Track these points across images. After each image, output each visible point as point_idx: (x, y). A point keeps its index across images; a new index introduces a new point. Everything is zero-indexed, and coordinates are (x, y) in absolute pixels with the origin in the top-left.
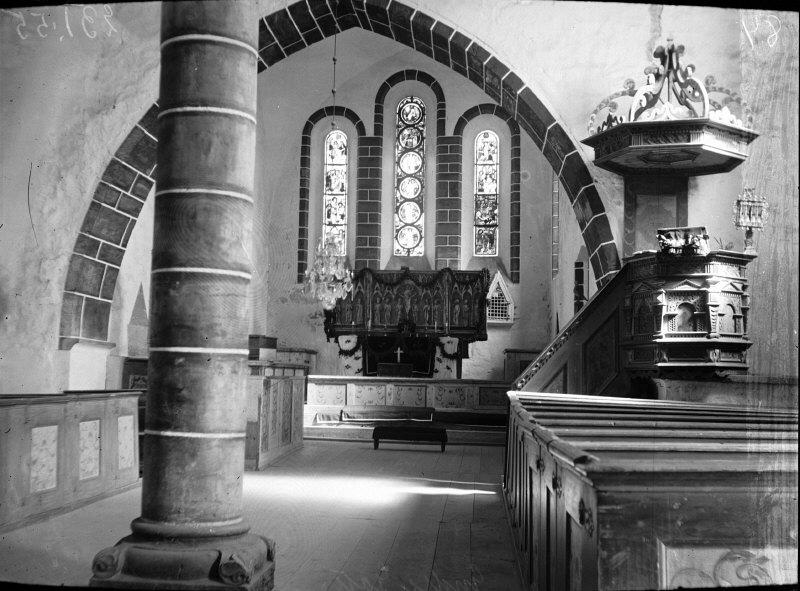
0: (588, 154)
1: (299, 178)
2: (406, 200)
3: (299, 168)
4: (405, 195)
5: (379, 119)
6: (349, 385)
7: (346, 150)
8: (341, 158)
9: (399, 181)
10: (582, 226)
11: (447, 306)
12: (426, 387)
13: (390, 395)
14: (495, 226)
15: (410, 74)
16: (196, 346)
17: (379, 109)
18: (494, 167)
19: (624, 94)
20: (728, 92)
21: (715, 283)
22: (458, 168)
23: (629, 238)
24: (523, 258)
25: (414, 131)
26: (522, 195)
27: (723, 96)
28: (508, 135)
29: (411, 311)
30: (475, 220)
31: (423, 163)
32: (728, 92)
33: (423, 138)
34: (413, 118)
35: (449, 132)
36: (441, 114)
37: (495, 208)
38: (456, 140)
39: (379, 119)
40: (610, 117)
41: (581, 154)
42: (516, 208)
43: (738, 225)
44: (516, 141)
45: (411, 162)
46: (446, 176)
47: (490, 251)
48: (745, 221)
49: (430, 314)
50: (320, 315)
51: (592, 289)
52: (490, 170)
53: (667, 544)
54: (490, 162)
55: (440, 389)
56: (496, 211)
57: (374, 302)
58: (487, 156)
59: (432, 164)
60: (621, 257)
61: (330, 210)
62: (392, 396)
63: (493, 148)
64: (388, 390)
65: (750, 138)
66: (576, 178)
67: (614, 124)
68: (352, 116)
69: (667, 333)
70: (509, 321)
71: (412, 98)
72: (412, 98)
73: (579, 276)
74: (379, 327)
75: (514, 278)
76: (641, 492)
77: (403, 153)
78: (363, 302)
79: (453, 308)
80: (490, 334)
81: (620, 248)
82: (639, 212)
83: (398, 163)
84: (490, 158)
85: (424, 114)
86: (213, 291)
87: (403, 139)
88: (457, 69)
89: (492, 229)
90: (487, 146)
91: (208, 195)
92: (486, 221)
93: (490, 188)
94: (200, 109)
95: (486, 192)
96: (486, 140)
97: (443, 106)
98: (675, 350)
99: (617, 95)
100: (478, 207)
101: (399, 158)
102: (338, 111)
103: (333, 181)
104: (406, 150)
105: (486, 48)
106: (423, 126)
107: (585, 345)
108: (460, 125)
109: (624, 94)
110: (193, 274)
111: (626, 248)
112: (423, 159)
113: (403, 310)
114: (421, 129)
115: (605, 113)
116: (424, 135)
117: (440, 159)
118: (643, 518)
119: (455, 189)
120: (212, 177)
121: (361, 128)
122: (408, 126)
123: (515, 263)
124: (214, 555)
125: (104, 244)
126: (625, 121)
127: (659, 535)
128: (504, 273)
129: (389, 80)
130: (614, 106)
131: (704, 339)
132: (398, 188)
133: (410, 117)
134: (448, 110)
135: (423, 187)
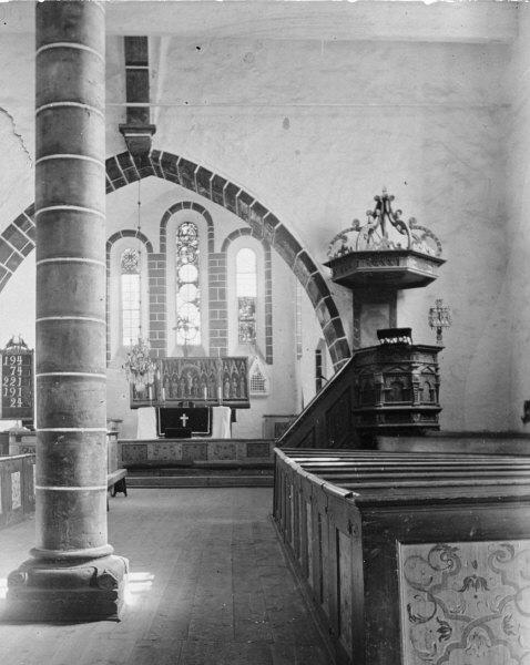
0: (327, 273)
10: (322, 325)
11: (220, 383)
14: (253, 320)
15: (187, 205)
16: (72, 427)
19: (352, 230)
20: (424, 229)
21: (416, 367)
22: (223, 277)
23: (357, 335)
24: (275, 345)
27: (422, 232)
32: (424, 229)
35: (218, 249)
38: (223, 256)
39: (163, 239)
40: (343, 247)
41: (322, 273)
42: (269, 308)
43: (432, 326)
44: (268, 256)
48: (436, 323)
51: (330, 373)
53: (402, 543)
59: (205, 275)
60: (351, 349)
65: (438, 262)
66: (320, 289)
67: (347, 252)
68: (143, 238)
69: (382, 405)
73: (319, 360)
75: (269, 361)
76: (387, 514)
80: (252, 403)
81: (350, 343)
82: (363, 316)
86: (83, 388)
88: (229, 208)
91: (76, 321)
94: (68, 259)
97: (212, 229)
98: (389, 414)
99: (348, 231)
100: (240, 307)
105: (251, 194)
107: (327, 412)
108: (226, 243)
109: (352, 230)
110: (68, 377)
111: (356, 343)
113: (186, 388)
115: (339, 243)
117: (211, 271)
118: (387, 528)
120: (76, 308)
121: (149, 247)
123: (270, 350)
124: (92, 571)
125: (38, 373)
126: (354, 250)
127: (399, 538)
128: (261, 356)
129: (170, 210)
130: (345, 239)
131: (410, 407)
134: (216, 232)
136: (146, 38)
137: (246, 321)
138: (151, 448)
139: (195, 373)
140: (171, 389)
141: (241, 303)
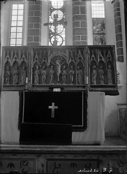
11: (87, 70)
29: (61, 75)
49: (74, 77)
57: (34, 69)
74: (37, 86)
89: (102, 35)
113: (55, 75)
136: (55, 106)
137: (98, 34)
139: (63, 61)
140: (40, 75)
141: (95, 21)
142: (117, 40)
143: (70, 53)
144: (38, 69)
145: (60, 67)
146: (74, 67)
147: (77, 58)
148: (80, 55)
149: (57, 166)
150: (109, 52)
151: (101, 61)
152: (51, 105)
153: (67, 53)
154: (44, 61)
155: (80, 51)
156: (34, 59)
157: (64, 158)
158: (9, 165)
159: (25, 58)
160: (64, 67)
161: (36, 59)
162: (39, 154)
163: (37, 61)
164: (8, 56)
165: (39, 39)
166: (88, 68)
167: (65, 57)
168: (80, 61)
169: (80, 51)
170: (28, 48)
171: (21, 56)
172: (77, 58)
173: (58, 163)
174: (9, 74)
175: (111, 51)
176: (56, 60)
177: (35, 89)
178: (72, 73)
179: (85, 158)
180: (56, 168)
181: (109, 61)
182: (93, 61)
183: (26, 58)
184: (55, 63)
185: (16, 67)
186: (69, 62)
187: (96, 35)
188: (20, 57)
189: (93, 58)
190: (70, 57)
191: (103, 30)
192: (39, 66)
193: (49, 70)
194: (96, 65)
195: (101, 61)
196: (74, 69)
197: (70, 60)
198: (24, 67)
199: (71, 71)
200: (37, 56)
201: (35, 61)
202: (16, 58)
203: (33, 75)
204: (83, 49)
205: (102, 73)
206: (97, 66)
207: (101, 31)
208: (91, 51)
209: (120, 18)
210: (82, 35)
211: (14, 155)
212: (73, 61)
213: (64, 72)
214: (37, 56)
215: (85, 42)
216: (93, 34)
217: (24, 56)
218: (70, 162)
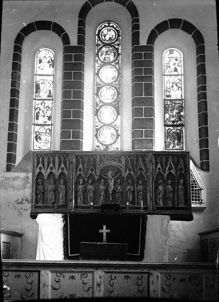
1: (10, 80)
2: (105, 104)
3: (11, 71)
4: (103, 99)
5: (81, 31)
6: (43, 272)
7: (53, 63)
8: (50, 71)
9: (99, 89)
12: (149, 274)
13: (99, 285)
14: (182, 125)
17: (81, 24)
18: (179, 77)
25: (110, 48)
26: (208, 95)
28: (193, 47)
29: (114, 191)
30: (165, 121)
31: (119, 74)
33: (119, 55)
34: (110, 39)
35: (143, 41)
36: (136, 27)
37: (181, 111)
38: (149, 48)
39: (81, 31)
45: (108, 74)
46: (142, 79)
47: (177, 147)
49: (133, 195)
50: (27, 200)
52: (176, 79)
54: (176, 73)
55: (168, 277)
56: (182, 114)
57: (77, 183)
58: (173, 68)
61: (38, 112)
62: (102, 286)
63: (177, 62)
64: (97, 279)
68: (58, 29)
70: (202, 205)
71: (109, 24)
72: (109, 24)
74: (82, 207)
77: (101, 66)
78: (65, 183)
79: (157, 188)
83: (98, 74)
84: (176, 70)
85: (119, 36)
87: (101, 55)
89: (179, 128)
90: (173, 61)
92: (173, 122)
93: (176, 94)
95: (173, 97)
96: (171, 56)
97: (138, 20)
101: (99, 70)
102: (43, 25)
103: (41, 89)
104: (105, 63)
106: (118, 45)
112: (118, 71)
113: (106, 191)
114: (117, 47)
116: (120, 52)
119: (149, 89)
121: (66, 39)
122: (105, 45)
132: (97, 94)
133: (107, 38)
134: (141, 24)
135: (119, 94)
138: (48, 277)
142: (200, 137)
143: (126, 161)
144: (83, 184)
145: (113, 181)
146: (133, 181)
147: (137, 169)
148: (141, 165)
149: (113, 278)
150: (181, 161)
151: (170, 173)
152: (107, 229)
153: (123, 162)
154: (90, 172)
155: (140, 159)
156: (77, 170)
157: (119, 271)
158: (70, 277)
159: (65, 168)
160: (119, 181)
161: (80, 170)
162: (97, 267)
163: (82, 173)
164: (40, 165)
165: (81, 135)
166: (152, 182)
167: (121, 168)
168: (141, 173)
169: (140, 159)
170: (68, 154)
171: (59, 166)
172: (137, 169)
173: (113, 275)
174: (42, 190)
175: (183, 159)
176: (108, 171)
177: (78, 211)
178: (130, 189)
179: (137, 271)
180: (112, 279)
181: (181, 174)
182: (159, 173)
183: (66, 168)
184: (107, 176)
185: (52, 180)
186: (125, 174)
187: (169, 128)
188: (57, 166)
189: (159, 169)
190: (126, 166)
191: (181, 120)
192: (84, 180)
193: (99, 186)
194: (162, 179)
195: (170, 173)
196: (133, 184)
197: (128, 172)
198: (62, 181)
199: (129, 187)
200: (81, 165)
201: (78, 173)
202: (51, 168)
203: (75, 192)
204: (146, 156)
205: (170, 191)
206: (164, 181)
207: (177, 121)
208: (156, 159)
209: (206, 102)
210: (145, 128)
211: (75, 269)
212: (132, 173)
213: (119, 188)
214: (81, 165)
215: (150, 141)
216: (165, 126)
217: (62, 166)
218: (124, 275)
